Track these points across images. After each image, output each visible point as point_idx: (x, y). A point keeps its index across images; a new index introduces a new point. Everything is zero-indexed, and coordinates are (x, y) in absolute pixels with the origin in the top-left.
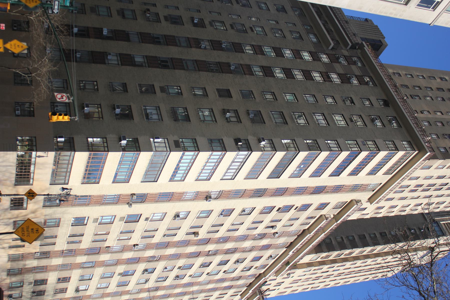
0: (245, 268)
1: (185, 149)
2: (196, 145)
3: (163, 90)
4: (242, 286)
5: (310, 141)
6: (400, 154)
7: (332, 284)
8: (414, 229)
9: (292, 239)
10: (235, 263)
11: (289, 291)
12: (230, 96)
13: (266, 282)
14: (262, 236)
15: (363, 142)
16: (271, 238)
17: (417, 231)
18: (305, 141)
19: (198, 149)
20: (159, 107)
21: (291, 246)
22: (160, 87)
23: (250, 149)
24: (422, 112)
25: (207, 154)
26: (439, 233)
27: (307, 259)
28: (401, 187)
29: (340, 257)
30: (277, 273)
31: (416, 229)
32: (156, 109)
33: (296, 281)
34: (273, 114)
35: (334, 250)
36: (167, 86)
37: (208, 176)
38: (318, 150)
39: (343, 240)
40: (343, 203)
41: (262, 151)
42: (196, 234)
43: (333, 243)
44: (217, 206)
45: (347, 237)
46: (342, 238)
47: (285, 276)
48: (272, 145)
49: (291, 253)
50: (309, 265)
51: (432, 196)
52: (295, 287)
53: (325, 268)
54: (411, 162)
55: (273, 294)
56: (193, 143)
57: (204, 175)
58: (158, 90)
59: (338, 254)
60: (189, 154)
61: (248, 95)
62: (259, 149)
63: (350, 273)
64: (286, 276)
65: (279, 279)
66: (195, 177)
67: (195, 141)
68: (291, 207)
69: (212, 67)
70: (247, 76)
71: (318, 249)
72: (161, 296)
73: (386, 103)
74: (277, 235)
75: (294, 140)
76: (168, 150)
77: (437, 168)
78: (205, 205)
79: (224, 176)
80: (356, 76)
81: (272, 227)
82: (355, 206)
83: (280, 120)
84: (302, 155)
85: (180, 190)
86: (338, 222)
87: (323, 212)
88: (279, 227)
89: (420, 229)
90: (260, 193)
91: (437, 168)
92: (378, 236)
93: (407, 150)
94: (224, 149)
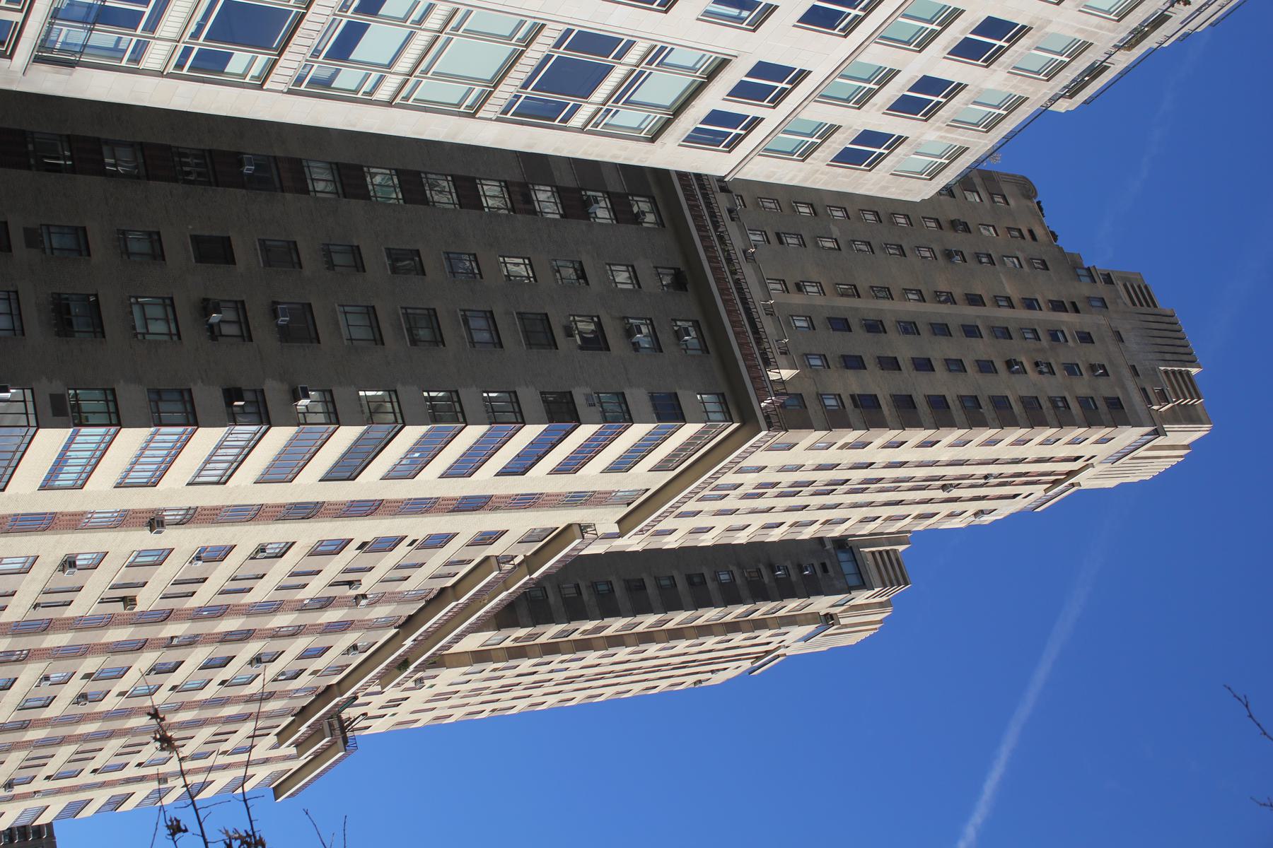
0: (283, 673)
1: (79, 420)
2: (112, 409)
3: (33, 238)
4: (281, 714)
5: (441, 394)
6: (689, 430)
7: (552, 701)
8: (786, 568)
9: (412, 609)
10: (251, 663)
11: (425, 719)
12: (229, 259)
13: (356, 698)
14: (325, 603)
15: (588, 397)
16: (350, 607)
17: (792, 572)
18: (426, 394)
19: (116, 419)
20: (16, 292)
21: (409, 624)
22: (25, 230)
23: (265, 419)
24: (799, 288)
25: (142, 434)
26: (853, 580)
27: (473, 642)
28: (716, 488)
29: (570, 638)
30: (385, 679)
31: (790, 566)
32: (9, 299)
33: (444, 696)
34: (345, 313)
35: (550, 620)
36: (48, 226)
37: (167, 455)
38: (458, 422)
39: (579, 593)
40: (545, 530)
41: (298, 425)
42: (129, 601)
43: (552, 599)
44: (184, 541)
45: (594, 585)
46: (577, 587)
47: (410, 684)
48: (330, 406)
49: (408, 643)
50: (480, 656)
51: (872, 464)
52: (442, 708)
53: (525, 665)
54: (669, 488)
55: (378, 727)
56: (107, 401)
57: (140, 475)
58: (17, 238)
59: (564, 631)
60: (91, 435)
61: (281, 255)
62: (292, 419)
63: (601, 676)
64: (413, 685)
65: (391, 692)
66: (116, 478)
67: (111, 396)
68: (395, 542)
69: (187, 164)
70: (288, 196)
71: (505, 618)
72: (38, 741)
73: (679, 282)
74: (364, 602)
75: (395, 392)
76: (33, 422)
77: (811, 448)
78: (145, 539)
79: (198, 475)
80: (610, 195)
81: (350, 583)
82: (578, 541)
83: (361, 333)
84: (411, 434)
85: (73, 508)
86: (535, 575)
87: (495, 550)
88: (368, 583)
89: (801, 568)
90: (306, 511)
91: (811, 448)
92: (682, 585)
93: (709, 420)
94: (193, 420)
